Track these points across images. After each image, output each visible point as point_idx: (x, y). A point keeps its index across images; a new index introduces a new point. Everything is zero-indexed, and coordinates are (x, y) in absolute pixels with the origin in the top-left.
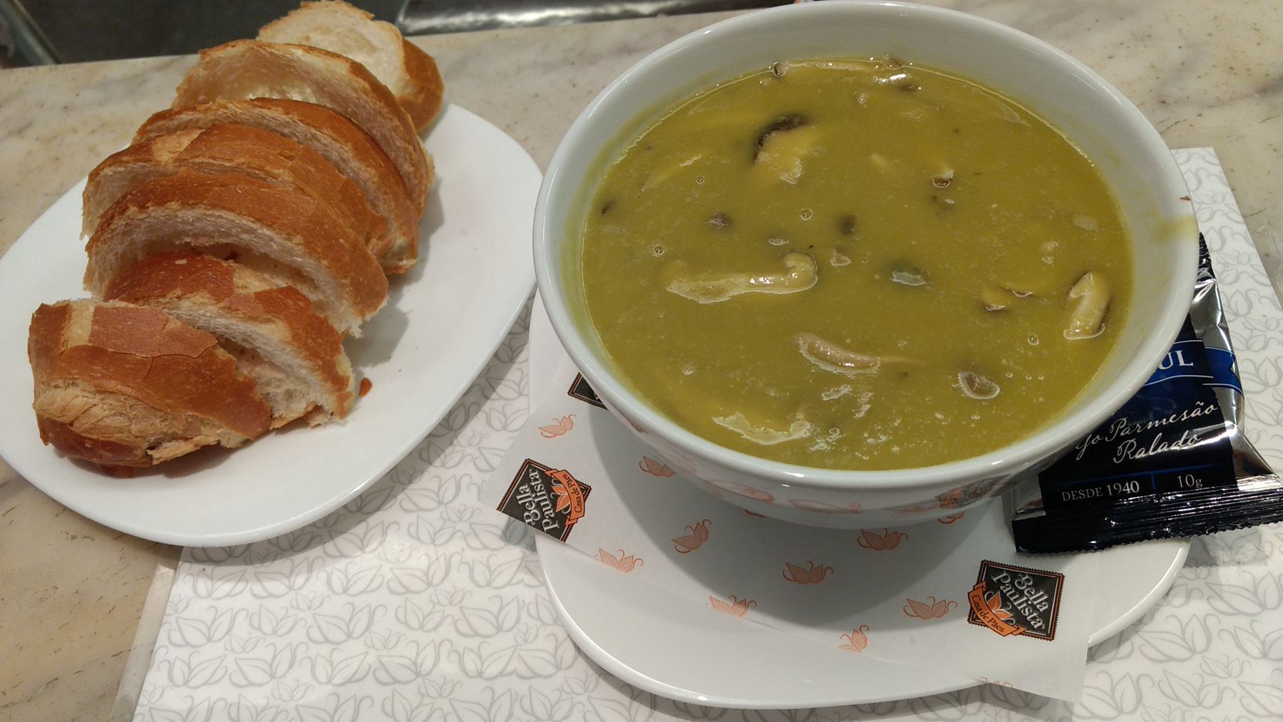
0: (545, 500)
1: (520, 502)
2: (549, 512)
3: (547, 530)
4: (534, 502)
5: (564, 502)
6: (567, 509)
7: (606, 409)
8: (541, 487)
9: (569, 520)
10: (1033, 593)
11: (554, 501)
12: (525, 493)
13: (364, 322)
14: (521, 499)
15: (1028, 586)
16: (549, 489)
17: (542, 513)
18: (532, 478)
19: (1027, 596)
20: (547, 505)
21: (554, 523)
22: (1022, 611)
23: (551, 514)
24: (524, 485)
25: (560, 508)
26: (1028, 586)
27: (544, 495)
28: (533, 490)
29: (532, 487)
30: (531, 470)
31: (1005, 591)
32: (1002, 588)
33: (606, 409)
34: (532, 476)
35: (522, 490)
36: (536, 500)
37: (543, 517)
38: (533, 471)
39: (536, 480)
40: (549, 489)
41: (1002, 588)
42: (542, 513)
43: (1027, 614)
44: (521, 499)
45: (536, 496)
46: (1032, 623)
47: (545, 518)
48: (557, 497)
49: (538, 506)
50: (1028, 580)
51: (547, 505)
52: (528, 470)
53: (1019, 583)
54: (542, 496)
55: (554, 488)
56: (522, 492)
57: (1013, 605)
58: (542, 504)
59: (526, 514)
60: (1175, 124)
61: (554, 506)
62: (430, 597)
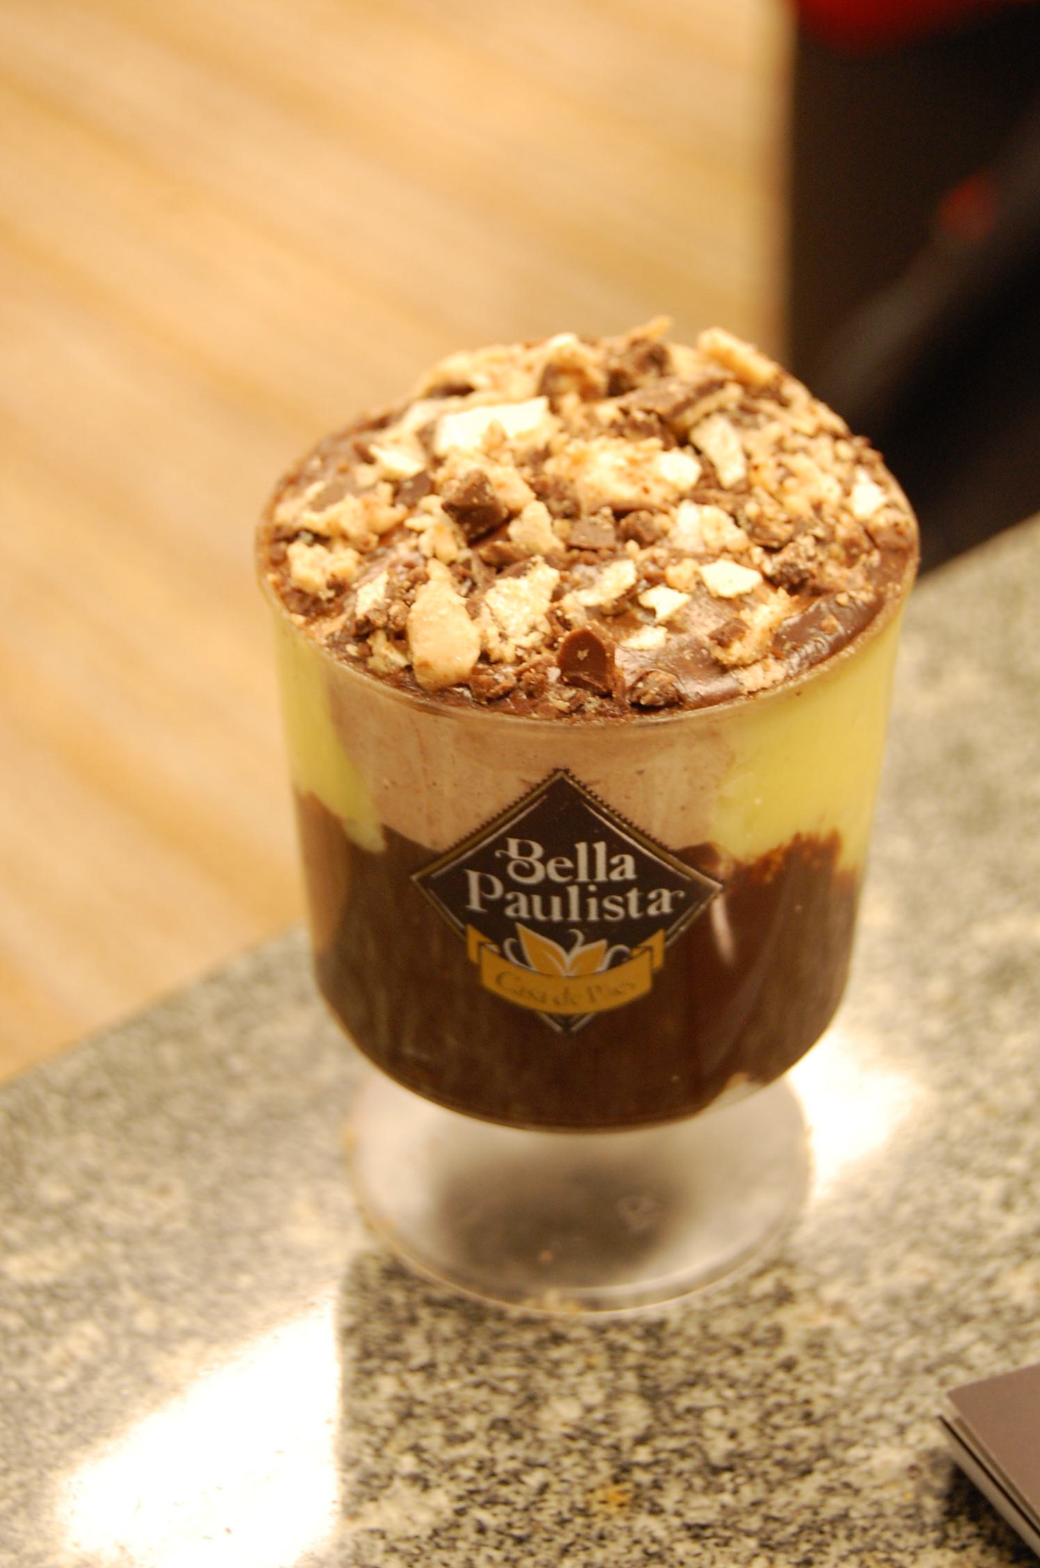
0: (565, 910)
4: (571, 883)
6: (518, 951)
9: (481, 944)
12: (610, 868)
23: (659, 908)
24: (637, 869)
25: (981, 1310)
28: (608, 889)
29: (624, 887)
36: (574, 892)
37: (510, 885)
38: (675, 902)
42: (529, 891)
47: (506, 891)
48: (568, 944)
49: (547, 889)
50: (525, 851)
53: (520, 870)
55: (603, 943)
56: (615, 860)
58: (556, 902)
60: (417, 730)
61: (532, 924)
62: (789, 1563)
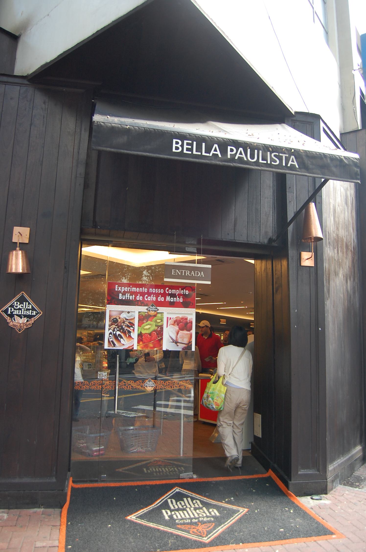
0: (21, 313)
1: (24, 303)
2: (16, 312)
3: (9, 309)
5: (18, 320)
6: (14, 319)
7: (356, 28)
8: (28, 314)
10: (22, 305)
11: (20, 316)
12: (28, 306)
13: (98, 322)
14: (26, 304)
15: (19, 305)
16: (25, 316)
17: (17, 309)
18: (33, 312)
19: (23, 308)
20: (19, 313)
21: (11, 312)
22: (29, 311)
26: (19, 305)
27: (24, 313)
28: (28, 310)
29: (29, 310)
30: (37, 312)
31: (16, 313)
32: (14, 313)
33: (356, 28)
34: (34, 312)
35: (30, 306)
36: (23, 309)
37: (15, 309)
39: (32, 313)
40: (25, 316)
41: (14, 313)
43: (28, 313)
44: (26, 304)
45: (24, 310)
46: (33, 314)
47: (14, 310)
48: (21, 318)
50: (17, 304)
51: (19, 313)
52: (37, 311)
53: (16, 307)
54: (23, 312)
56: (29, 305)
57: (22, 315)
59: (19, 303)
